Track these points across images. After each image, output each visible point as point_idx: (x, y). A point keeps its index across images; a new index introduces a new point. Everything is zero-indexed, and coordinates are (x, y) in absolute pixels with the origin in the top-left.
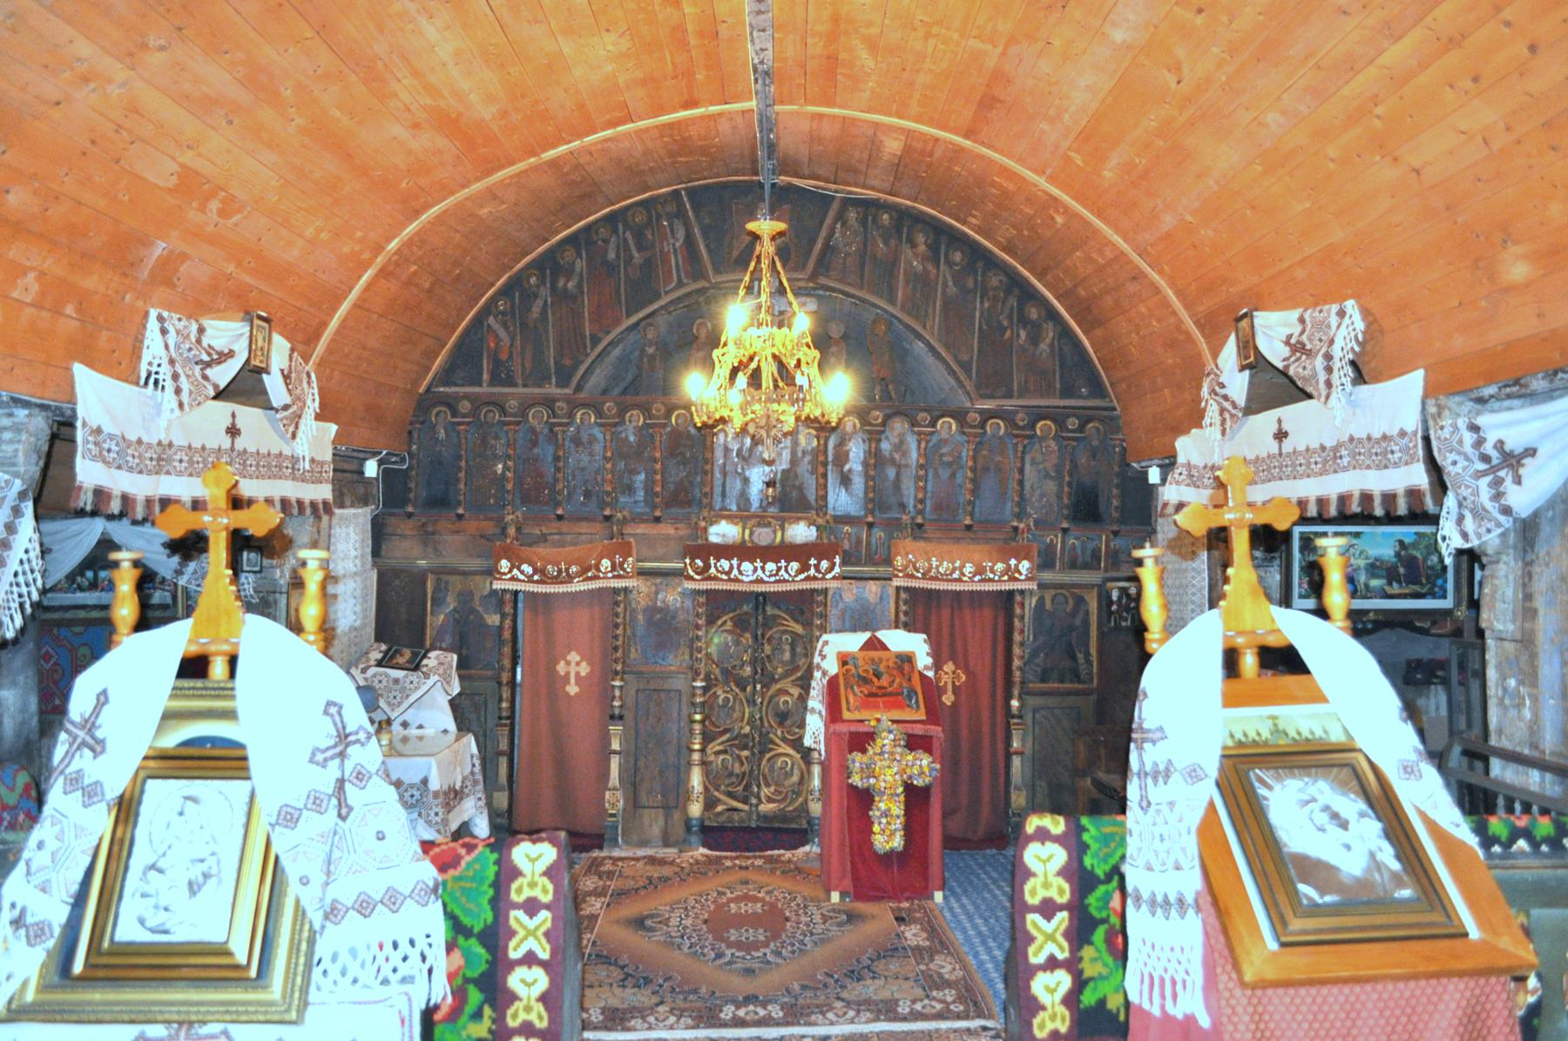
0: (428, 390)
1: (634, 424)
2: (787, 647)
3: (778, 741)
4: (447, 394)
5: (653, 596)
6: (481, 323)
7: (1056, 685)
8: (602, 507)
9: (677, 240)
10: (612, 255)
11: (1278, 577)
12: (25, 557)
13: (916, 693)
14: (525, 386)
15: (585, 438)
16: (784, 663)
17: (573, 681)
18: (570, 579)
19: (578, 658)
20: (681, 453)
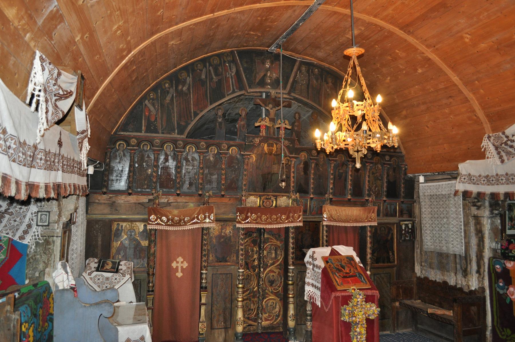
0: (115, 133)
1: (213, 153)
2: (273, 252)
3: (269, 293)
4: (125, 136)
5: (220, 230)
6: (142, 104)
7: (382, 264)
8: (197, 190)
9: (232, 72)
10: (203, 77)
11: (499, 221)
12: (30, 241)
13: (362, 275)
14: (163, 133)
15: (190, 158)
16: (272, 259)
17: (180, 270)
18: (185, 224)
19: (182, 260)
20: (233, 166)
